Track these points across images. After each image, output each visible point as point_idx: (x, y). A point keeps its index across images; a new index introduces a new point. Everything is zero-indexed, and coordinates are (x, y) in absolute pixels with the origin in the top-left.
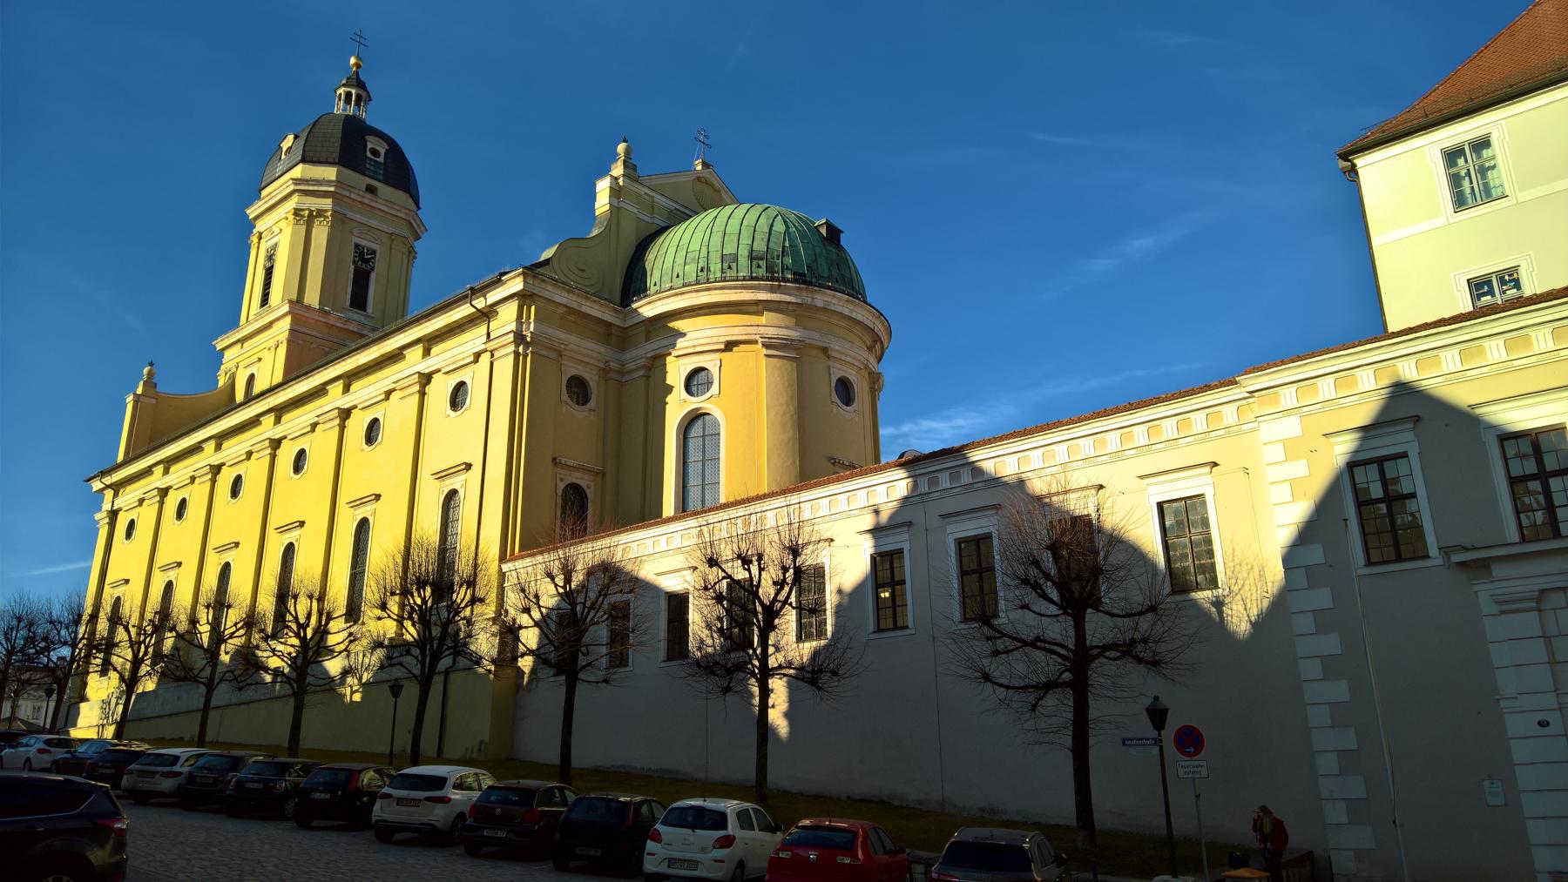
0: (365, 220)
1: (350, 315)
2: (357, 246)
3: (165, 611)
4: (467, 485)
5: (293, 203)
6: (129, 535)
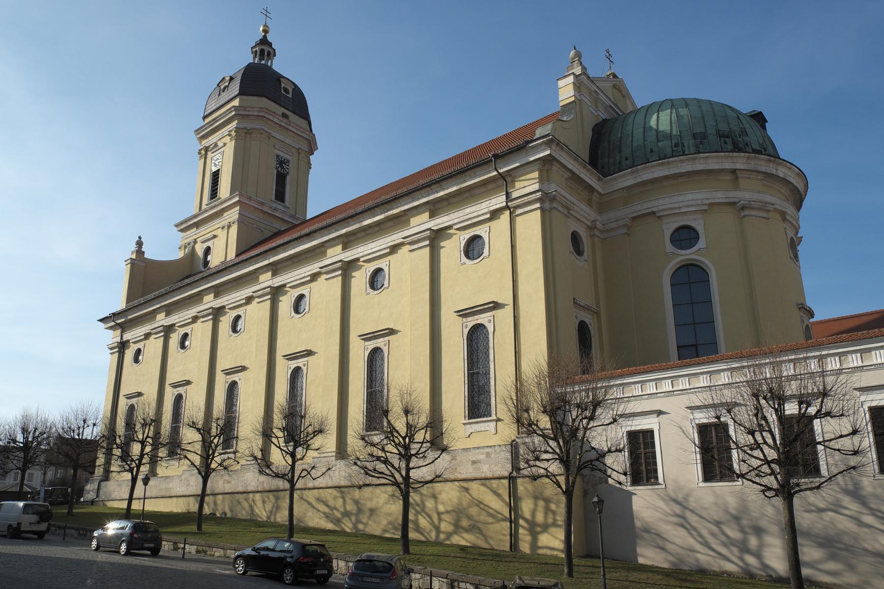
0: (282, 138)
1: (275, 205)
2: (278, 156)
3: (294, 412)
4: (499, 326)
5: (234, 124)
6: (136, 360)
